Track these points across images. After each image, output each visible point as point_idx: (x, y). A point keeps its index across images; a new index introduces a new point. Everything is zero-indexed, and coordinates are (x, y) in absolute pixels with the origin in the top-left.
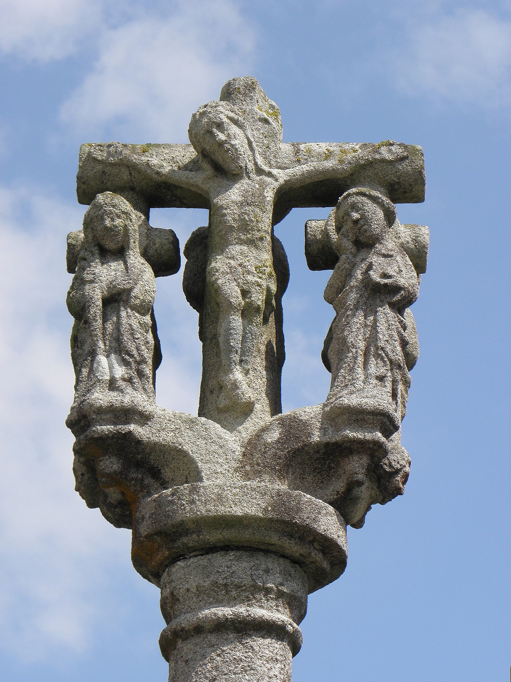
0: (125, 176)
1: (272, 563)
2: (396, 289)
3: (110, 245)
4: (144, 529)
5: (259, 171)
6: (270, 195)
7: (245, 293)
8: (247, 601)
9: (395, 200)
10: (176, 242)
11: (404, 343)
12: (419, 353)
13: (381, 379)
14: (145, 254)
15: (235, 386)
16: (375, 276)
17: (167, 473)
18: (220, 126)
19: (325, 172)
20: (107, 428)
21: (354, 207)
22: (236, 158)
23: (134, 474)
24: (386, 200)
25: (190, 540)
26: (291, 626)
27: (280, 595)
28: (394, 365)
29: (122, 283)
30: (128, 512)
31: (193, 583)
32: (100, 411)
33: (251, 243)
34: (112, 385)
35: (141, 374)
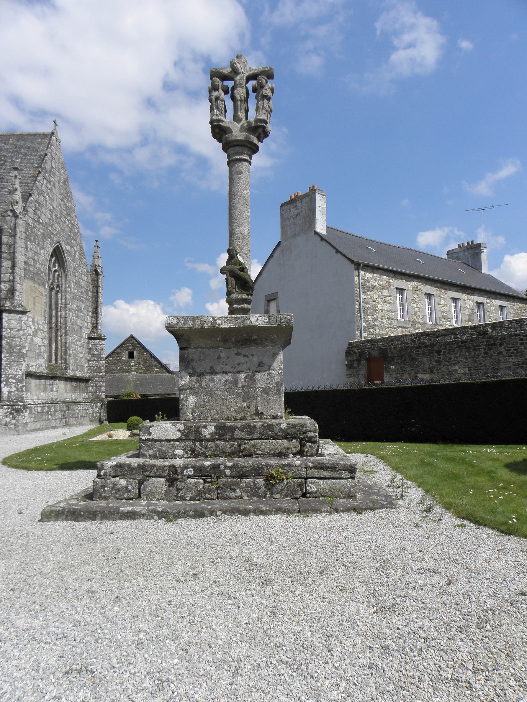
0: (218, 74)
1: (244, 148)
2: (267, 96)
3: (216, 88)
4: (223, 143)
5: (243, 73)
6: (245, 78)
7: (240, 97)
8: (241, 155)
9: (268, 79)
10: (228, 88)
11: (269, 107)
12: (273, 109)
13: (265, 114)
14: (222, 90)
15: (239, 115)
16: (264, 93)
17: (227, 132)
18: (235, 63)
19: (255, 73)
20: (216, 123)
21: (260, 80)
22: (238, 70)
23: (221, 132)
24: (266, 78)
25: (231, 144)
26: (249, 160)
27: (247, 154)
28: (267, 111)
29: (218, 95)
30: (502, 497)
31: (232, 152)
32: (215, 120)
33: (241, 87)
34: (217, 115)
35: (222, 113)
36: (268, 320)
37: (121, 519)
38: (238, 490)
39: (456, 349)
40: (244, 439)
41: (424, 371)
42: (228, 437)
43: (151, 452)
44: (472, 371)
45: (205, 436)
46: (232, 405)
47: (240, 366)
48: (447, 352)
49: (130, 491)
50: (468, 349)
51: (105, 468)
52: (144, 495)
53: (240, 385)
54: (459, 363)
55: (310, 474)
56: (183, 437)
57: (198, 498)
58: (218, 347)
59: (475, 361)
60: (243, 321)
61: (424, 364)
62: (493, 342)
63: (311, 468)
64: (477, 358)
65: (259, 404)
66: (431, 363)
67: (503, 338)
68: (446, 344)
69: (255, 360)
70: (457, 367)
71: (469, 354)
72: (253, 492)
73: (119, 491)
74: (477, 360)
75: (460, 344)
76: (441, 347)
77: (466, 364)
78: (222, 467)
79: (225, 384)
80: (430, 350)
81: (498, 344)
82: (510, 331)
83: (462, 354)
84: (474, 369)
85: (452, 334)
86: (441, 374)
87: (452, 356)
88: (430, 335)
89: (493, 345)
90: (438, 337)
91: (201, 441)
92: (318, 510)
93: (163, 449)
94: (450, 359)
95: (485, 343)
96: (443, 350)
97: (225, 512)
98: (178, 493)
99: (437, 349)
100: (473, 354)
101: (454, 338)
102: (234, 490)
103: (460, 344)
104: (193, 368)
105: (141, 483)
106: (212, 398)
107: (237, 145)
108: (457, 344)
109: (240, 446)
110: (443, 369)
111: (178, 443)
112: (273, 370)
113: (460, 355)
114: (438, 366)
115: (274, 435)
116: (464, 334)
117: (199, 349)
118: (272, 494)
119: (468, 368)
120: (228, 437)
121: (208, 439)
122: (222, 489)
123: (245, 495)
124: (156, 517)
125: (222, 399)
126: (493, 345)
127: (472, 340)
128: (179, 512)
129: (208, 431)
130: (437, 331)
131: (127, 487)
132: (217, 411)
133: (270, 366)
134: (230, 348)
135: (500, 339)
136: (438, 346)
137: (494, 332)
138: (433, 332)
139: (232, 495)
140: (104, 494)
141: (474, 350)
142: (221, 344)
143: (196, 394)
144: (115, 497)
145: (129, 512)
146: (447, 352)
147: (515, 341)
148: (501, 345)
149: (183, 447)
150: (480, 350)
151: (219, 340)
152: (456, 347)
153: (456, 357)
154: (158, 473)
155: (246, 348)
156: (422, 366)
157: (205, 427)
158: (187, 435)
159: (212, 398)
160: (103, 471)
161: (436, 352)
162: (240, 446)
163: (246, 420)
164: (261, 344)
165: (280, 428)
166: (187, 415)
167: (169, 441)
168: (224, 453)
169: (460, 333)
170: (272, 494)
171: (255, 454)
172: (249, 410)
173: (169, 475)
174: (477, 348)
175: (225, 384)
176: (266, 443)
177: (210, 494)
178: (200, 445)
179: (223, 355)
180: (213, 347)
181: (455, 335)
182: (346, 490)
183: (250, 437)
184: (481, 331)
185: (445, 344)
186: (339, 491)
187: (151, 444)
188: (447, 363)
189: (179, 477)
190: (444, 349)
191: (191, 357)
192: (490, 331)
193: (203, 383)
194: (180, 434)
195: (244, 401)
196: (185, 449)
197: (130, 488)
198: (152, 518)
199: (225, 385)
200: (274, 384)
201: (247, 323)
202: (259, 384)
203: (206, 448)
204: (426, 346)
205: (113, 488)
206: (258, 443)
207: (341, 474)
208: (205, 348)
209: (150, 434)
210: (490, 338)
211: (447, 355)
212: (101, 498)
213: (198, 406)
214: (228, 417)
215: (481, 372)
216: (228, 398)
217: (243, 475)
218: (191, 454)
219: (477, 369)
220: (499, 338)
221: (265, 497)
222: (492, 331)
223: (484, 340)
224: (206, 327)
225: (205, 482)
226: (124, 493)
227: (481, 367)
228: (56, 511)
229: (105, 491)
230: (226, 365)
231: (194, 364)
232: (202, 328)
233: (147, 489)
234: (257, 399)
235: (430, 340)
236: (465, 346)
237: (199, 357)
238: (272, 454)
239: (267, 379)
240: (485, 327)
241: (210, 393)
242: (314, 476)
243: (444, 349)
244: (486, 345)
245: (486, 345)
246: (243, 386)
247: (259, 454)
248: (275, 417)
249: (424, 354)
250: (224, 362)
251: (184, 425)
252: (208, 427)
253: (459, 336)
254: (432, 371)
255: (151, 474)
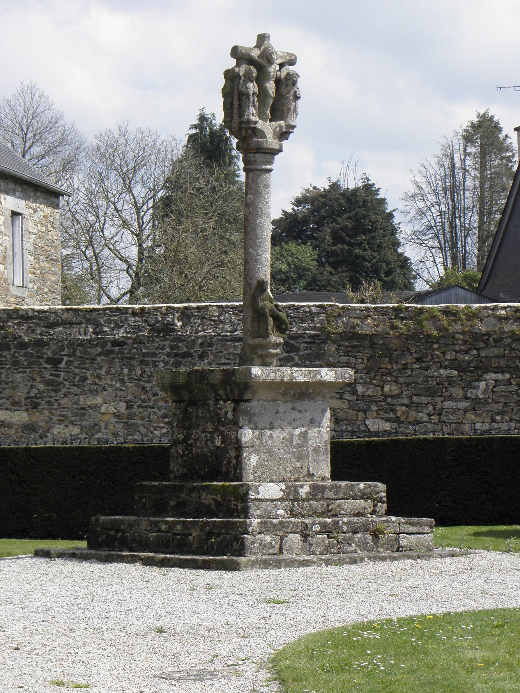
17: (257, 134)
25: (262, 151)
36: (334, 375)
37: (299, 567)
38: (353, 545)
39: (99, 359)
40: (332, 499)
41: (14, 404)
42: (319, 497)
43: (258, 512)
44: (135, 409)
45: (301, 496)
46: (288, 465)
47: (296, 421)
48: (76, 364)
49: (274, 547)
50: (127, 360)
51: (253, 525)
52: (286, 550)
53: (295, 443)
54: (104, 389)
55: (403, 529)
56: (285, 496)
57: (325, 552)
58: (277, 400)
59: (144, 388)
60: (315, 375)
61: (14, 388)
62: (185, 350)
63: (403, 524)
64: (148, 382)
65: (311, 465)
66: (32, 386)
67: (208, 343)
68: (74, 345)
69: (308, 416)
70: (99, 400)
71: (130, 371)
72: (364, 545)
73: (265, 547)
74: (148, 385)
75: (109, 347)
76: (63, 350)
77: (120, 393)
78: (341, 522)
79: (282, 442)
80: (32, 355)
81: (196, 355)
82: (223, 330)
83: (113, 371)
84: (139, 406)
85: (89, 321)
86: (58, 412)
87: (88, 374)
88: (31, 318)
89: (185, 355)
90: (52, 326)
91: (297, 500)
92: (431, 556)
93: (268, 508)
94: (85, 379)
95: (168, 350)
96: (65, 359)
97: (370, 559)
98: (310, 548)
99: (50, 354)
100: (139, 372)
101: (95, 333)
102: (350, 545)
103: (109, 347)
104: (255, 423)
105: (282, 539)
106: (271, 457)
107: (268, 153)
108: (103, 347)
109: (328, 505)
110: (64, 401)
111: (279, 503)
112: (322, 427)
113: (108, 372)
114: (53, 394)
115: (354, 495)
116: (118, 326)
117: (261, 402)
118: (377, 548)
119: (127, 402)
120: (319, 497)
121: (304, 499)
122: (342, 543)
123: (358, 549)
124: (324, 564)
125: (280, 458)
126: (185, 355)
127: (139, 341)
128: (339, 559)
129: (304, 491)
130: (49, 311)
131: (271, 543)
132: (275, 472)
133: (320, 423)
134: (287, 402)
135: (201, 345)
136: (53, 347)
137: (188, 328)
138: (39, 312)
139: (349, 549)
140: (254, 550)
141: (142, 363)
142: (281, 397)
143: (257, 452)
144: (262, 552)
145: (304, 560)
146: (76, 364)
147: (231, 350)
148: (202, 357)
149: (284, 507)
150: (155, 364)
151: (280, 393)
152: (99, 355)
153: (99, 377)
154: (293, 530)
155: (300, 402)
156: (8, 392)
157: (302, 487)
158: (288, 494)
159: (271, 457)
160: (251, 528)
161: (49, 361)
162: (328, 505)
163: (300, 481)
164: (313, 399)
165: (359, 488)
166: (249, 476)
167: (273, 500)
168: (316, 513)
169: (109, 321)
170: (377, 548)
171: (340, 514)
172: (302, 471)
173: (302, 531)
174: (148, 359)
175: (282, 442)
176: (348, 503)
177: (334, 549)
178: (298, 505)
179: (281, 409)
180: (273, 401)
181: (97, 325)
182: (427, 543)
183: (336, 497)
184: (157, 322)
185: (71, 344)
186: (422, 545)
187: (258, 504)
188: (75, 390)
189: (311, 533)
190: (69, 356)
191: (253, 411)
192: (179, 324)
193: (264, 441)
194: (282, 493)
195: (298, 461)
196: (286, 509)
197: (273, 543)
198: (321, 565)
199: (282, 443)
200: (323, 443)
201: (318, 377)
202: (310, 443)
203: (302, 508)
204: (23, 345)
205: (260, 544)
206: (342, 503)
207: (424, 529)
208: (266, 401)
209: (258, 493)
210: (180, 339)
211: (77, 371)
212: (252, 554)
213: (259, 465)
214: (284, 478)
215: (155, 413)
216: (285, 457)
217: (355, 531)
218: (291, 514)
219: (147, 407)
220: (200, 341)
221: (373, 550)
222: (183, 326)
223: (167, 343)
224: (286, 380)
225: (329, 537)
226: (269, 549)
227: (155, 401)
228: (252, 560)
229: (254, 547)
230: (283, 420)
231: (256, 419)
232: (282, 380)
233: (287, 545)
234: (308, 459)
235: (33, 331)
236: (121, 352)
237: (261, 411)
238: (353, 514)
239: (318, 437)
240: (166, 315)
241: (269, 452)
242: (405, 531)
243: (69, 356)
244: (169, 355)
245: (169, 355)
246: (297, 444)
247: (343, 514)
248: (323, 479)
249: (16, 363)
250: (281, 417)
251: (285, 484)
252: (305, 487)
253: (105, 329)
254: (35, 406)
255: (288, 531)
